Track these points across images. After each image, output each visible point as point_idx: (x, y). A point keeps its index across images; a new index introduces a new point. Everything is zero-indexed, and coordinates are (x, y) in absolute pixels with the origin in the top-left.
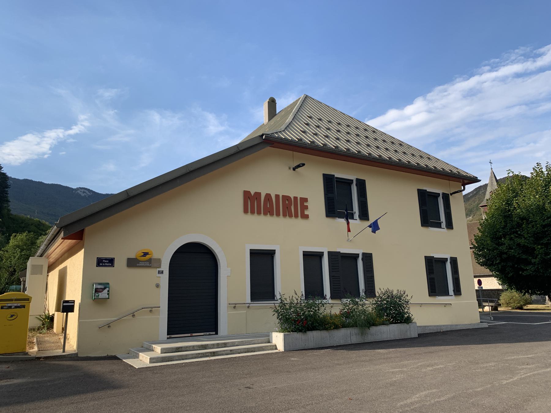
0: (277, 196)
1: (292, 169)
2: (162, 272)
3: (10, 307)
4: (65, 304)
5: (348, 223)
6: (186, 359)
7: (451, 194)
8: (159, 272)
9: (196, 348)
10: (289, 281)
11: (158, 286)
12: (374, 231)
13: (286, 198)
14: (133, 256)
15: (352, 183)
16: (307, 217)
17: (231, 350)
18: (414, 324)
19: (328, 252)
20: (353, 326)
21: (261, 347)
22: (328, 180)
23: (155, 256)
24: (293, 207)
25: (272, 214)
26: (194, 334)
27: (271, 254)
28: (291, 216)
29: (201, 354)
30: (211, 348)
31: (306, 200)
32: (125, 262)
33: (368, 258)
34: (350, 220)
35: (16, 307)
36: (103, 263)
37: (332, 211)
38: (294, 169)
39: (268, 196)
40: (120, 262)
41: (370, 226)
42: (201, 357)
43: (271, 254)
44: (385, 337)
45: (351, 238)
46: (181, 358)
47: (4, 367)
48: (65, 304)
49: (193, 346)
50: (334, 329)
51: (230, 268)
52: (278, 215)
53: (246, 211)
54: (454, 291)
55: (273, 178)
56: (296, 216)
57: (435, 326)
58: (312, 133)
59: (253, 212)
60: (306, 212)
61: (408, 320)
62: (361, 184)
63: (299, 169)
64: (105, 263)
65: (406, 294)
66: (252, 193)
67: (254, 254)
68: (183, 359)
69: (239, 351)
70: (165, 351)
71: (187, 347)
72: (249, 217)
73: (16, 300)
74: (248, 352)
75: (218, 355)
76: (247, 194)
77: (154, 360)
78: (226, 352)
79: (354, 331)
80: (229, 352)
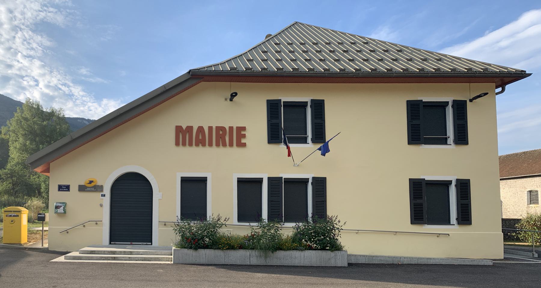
0: (210, 128)
1: (229, 100)
2: (104, 196)
3: (11, 216)
5: (288, 148)
7: (471, 101)
10: (222, 204)
11: (101, 205)
12: (323, 154)
13: (220, 129)
14: (83, 184)
15: (307, 105)
16: (244, 145)
17: (129, 258)
18: (342, 253)
19: (269, 178)
20: (253, 249)
21: (158, 258)
22: (273, 107)
23: (99, 183)
24: (234, 137)
25: (204, 145)
26: (133, 243)
28: (224, 145)
30: (118, 254)
31: (244, 129)
32: (77, 188)
33: (320, 184)
34: (291, 146)
35: (14, 216)
37: (274, 137)
38: (231, 100)
40: (74, 188)
41: (320, 149)
42: (104, 260)
44: (296, 263)
45: (297, 161)
47: (2, 251)
50: (226, 249)
51: (161, 193)
52: (211, 145)
53: (177, 144)
54: (457, 219)
55: (209, 111)
56: (231, 145)
57: (389, 257)
58: (421, 59)
59: (184, 144)
60: (243, 141)
61: (335, 247)
62: (319, 107)
63: (235, 99)
65: (337, 220)
66: (184, 128)
67: (241, 182)
72: (181, 148)
73: (14, 211)
74: (145, 260)
75: (118, 260)
76: (179, 129)
79: (254, 253)
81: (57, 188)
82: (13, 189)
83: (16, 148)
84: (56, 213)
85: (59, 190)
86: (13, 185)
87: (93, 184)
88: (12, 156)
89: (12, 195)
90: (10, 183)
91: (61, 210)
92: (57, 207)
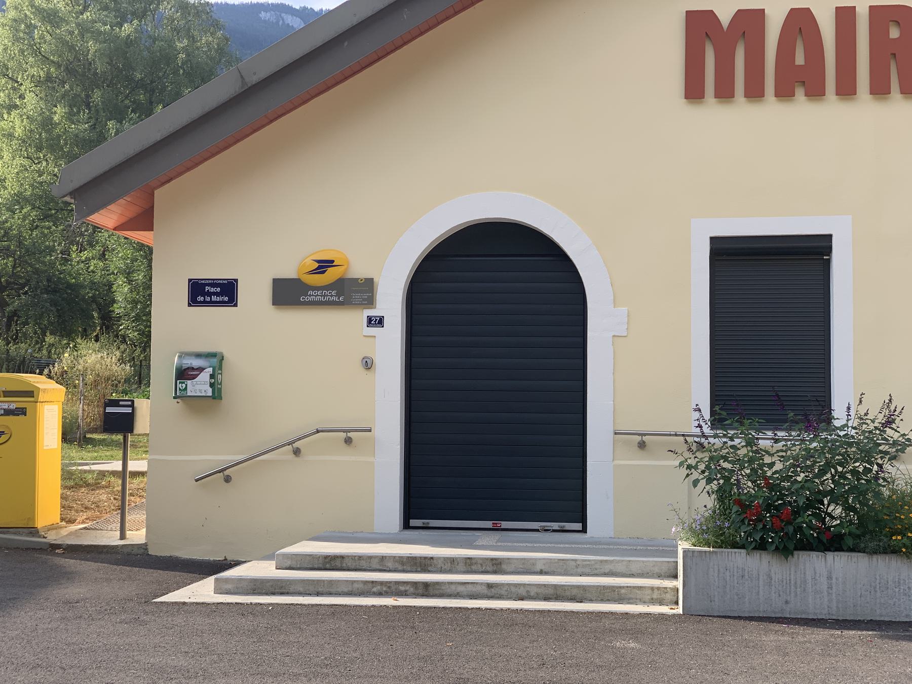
0: (845, 16)
2: (379, 322)
4: (109, 410)
6: (330, 594)
8: (370, 321)
9: (390, 565)
11: (368, 364)
14: (289, 272)
17: (490, 586)
21: (613, 588)
23: (358, 270)
25: (816, 92)
26: (505, 524)
27: (814, 252)
29: (382, 583)
30: (441, 571)
32: (266, 292)
36: (204, 294)
39: (801, 22)
40: (254, 293)
42: (380, 594)
43: (814, 252)
46: (312, 589)
48: (109, 410)
49: (383, 558)
51: (624, 309)
52: (846, 89)
53: (693, 91)
59: (725, 93)
64: (210, 294)
68: (318, 594)
69: (522, 592)
70: (288, 563)
71: (360, 558)
74: (558, 598)
75: (441, 596)
77: (229, 586)
78: (470, 588)
80: (484, 590)
84: (180, 396)
85: (193, 301)
87: (332, 275)
91: (200, 386)
92: (184, 374)
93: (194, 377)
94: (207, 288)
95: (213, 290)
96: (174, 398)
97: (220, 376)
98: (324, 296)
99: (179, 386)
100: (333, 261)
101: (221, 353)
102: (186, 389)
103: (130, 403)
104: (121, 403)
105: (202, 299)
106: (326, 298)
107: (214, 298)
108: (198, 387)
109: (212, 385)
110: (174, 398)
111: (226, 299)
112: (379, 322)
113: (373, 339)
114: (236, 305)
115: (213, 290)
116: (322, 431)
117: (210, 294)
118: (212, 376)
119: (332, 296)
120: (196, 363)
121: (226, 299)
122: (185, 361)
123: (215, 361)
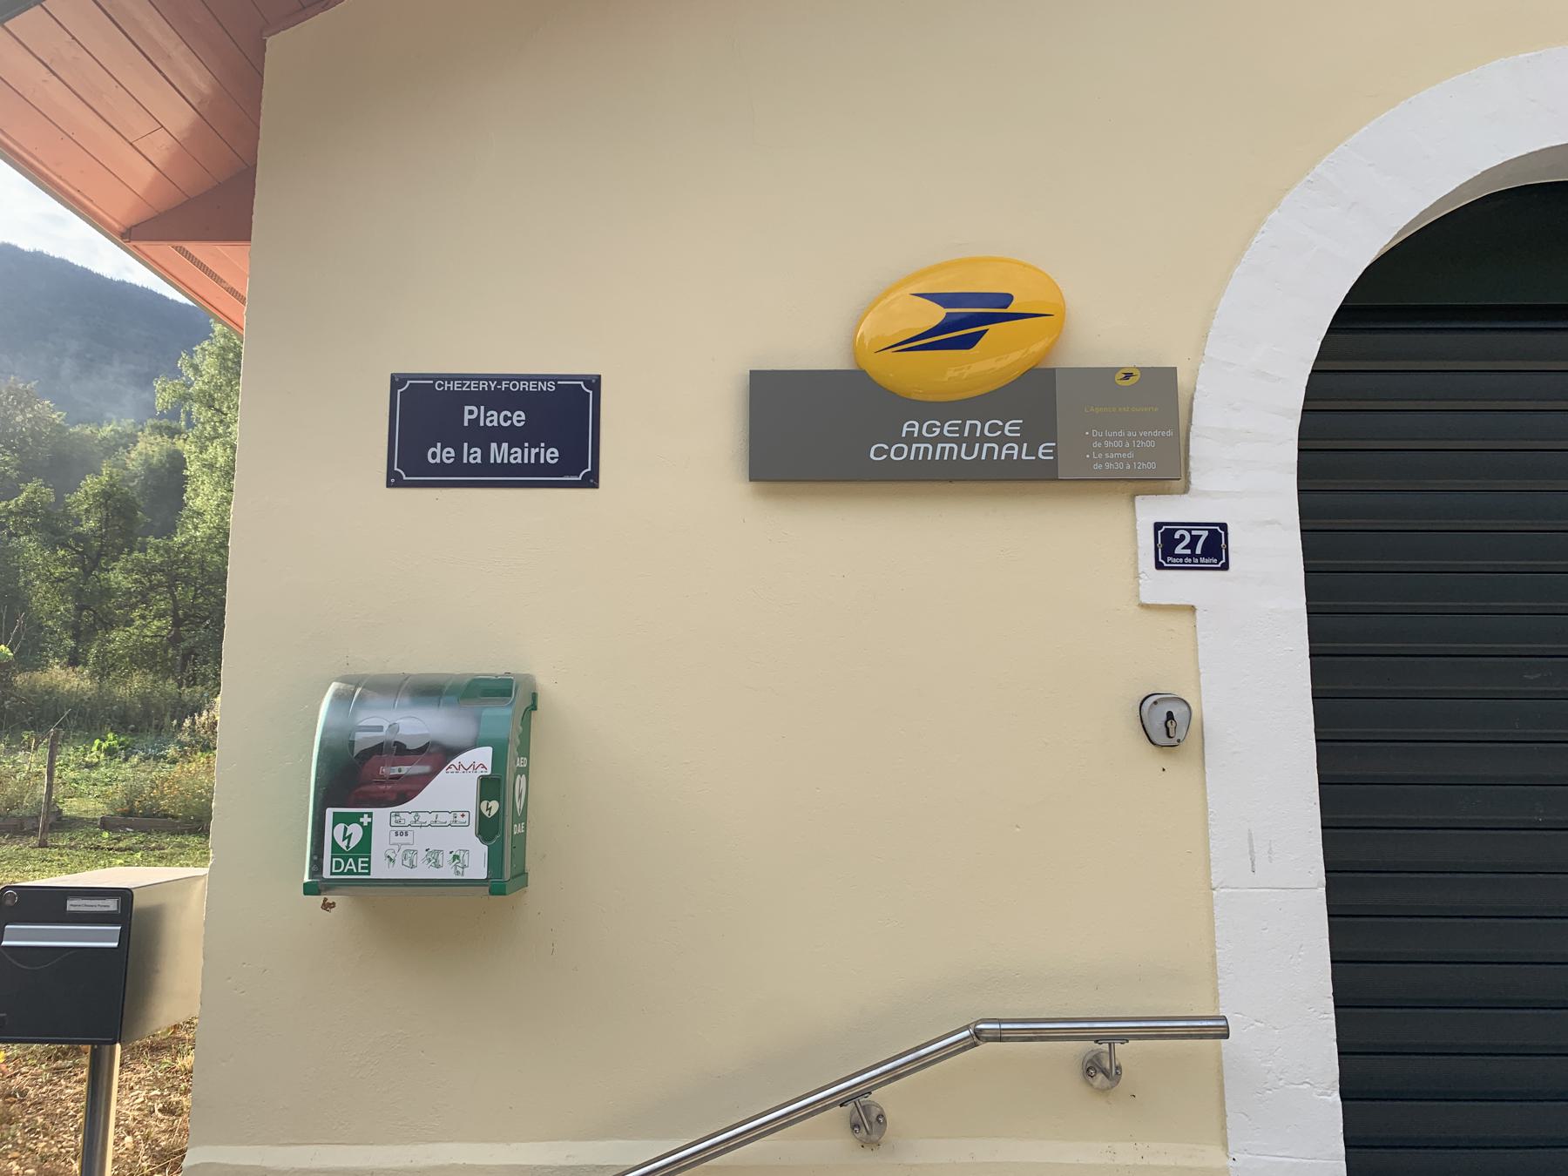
2: (1211, 548)
11: (1166, 726)
23: (1104, 330)
32: (722, 430)
36: (457, 435)
40: (671, 435)
64: (483, 436)
81: (371, 431)
82: (175, 640)
83: (211, 466)
84: (336, 877)
85: (409, 465)
86: (177, 623)
87: (998, 356)
88: (198, 503)
89: (167, 672)
90: (160, 615)
91: (432, 832)
92: (360, 777)
93: (404, 791)
94: (470, 413)
95: (494, 419)
96: (309, 890)
97: (521, 779)
98: (971, 441)
99: (334, 833)
100: (1007, 299)
101: (529, 680)
102: (365, 846)
103: (111, 905)
104: (73, 905)
105: (445, 455)
106: (981, 452)
107: (500, 453)
108: (423, 839)
109: (488, 829)
110: (309, 890)
111: (551, 455)
112: (1211, 548)
113: (1179, 623)
114: (591, 481)
115: (494, 419)
116: (999, 1037)
117: (483, 436)
118: (490, 787)
119: (1002, 441)
120: (418, 724)
121: (551, 455)
122: (367, 718)
123: (500, 715)
